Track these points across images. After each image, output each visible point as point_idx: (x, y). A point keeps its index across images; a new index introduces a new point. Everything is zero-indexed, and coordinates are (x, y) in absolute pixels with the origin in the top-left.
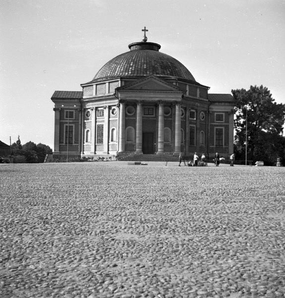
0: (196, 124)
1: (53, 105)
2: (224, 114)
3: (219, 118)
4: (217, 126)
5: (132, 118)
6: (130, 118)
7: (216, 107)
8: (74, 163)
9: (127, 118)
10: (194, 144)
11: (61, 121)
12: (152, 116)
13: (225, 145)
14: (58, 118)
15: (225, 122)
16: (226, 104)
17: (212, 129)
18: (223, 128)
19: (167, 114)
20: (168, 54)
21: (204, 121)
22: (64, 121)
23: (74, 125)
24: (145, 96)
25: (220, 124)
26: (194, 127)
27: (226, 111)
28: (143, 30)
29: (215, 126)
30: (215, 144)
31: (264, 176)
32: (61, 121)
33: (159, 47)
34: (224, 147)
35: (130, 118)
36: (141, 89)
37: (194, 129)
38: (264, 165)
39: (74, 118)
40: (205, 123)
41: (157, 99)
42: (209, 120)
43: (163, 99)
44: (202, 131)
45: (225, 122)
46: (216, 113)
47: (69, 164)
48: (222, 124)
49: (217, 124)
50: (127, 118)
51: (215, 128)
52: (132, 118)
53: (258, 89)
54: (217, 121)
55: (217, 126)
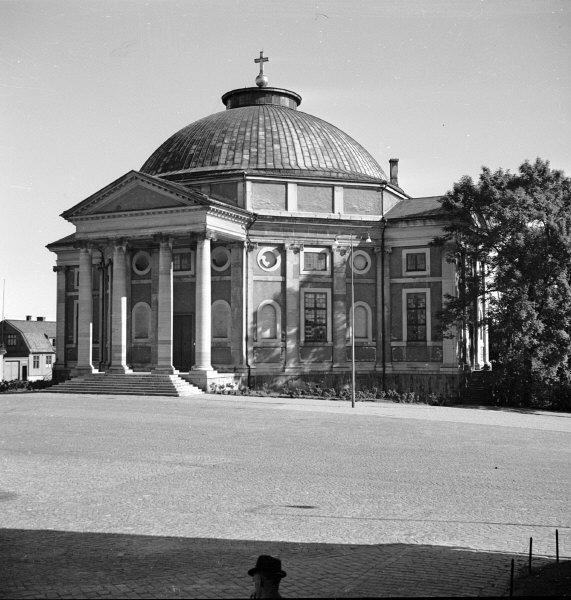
1: (52, 258)
4: (411, 286)
5: (146, 282)
6: (143, 282)
7: (404, 234)
8: (85, 395)
9: (134, 282)
11: (70, 294)
12: (187, 273)
13: (434, 338)
14: (63, 287)
15: (433, 275)
16: (428, 223)
18: (428, 291)
19: (221, 266)
21: (367, 276)
24: (127, 225)
25: (417, 280)
26: (408, 295)
28: (256, 61)
29: (405, 285)
30: (405, 338)
31: (553, 424)
32: (70, 294)
34: (429, 343)
35: (143, 282)
36: (119, 209)
38: (242, 392)
40: (370, 281)
41: (151, 232)
42: (387, 270)
43: (164, 231)
45: (433, 275)
46: (405, 253)
47: (33, 398)
48: (422, 280)
50: (134, 282)
51: (405, 292)
52: (146, 282)
53: (530, 168)
54: (410, 274)
55: (411, 286)
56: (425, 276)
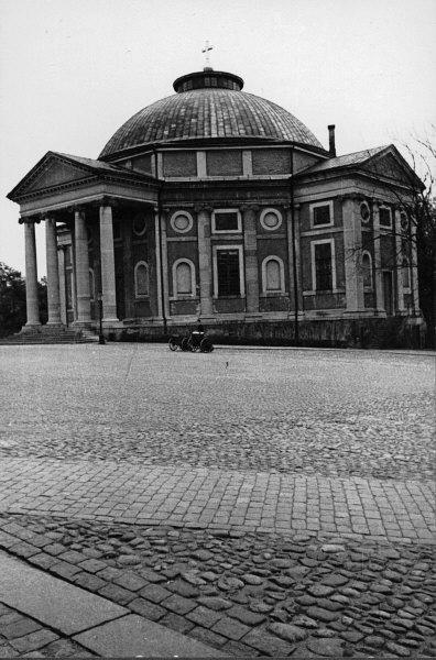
0: (242, 242)
2: (331, 203)
3: (322, 215)
9: (195, 239)
10: (332, 289)
13: (338, 287)
15: (335, 226)
17: (304, 248)
20: (24, 252)
22: (307, 234)
23: (331, 241)
25: (322, 232)
27: (334, 194)
30: (314, 287)
33: (239, 83)
34: (335, 291)
37: (237, 257)
39: (332, 223)
44: (144, 263)
45: (335, 226)
49: (318, 233)
56: (329, 228)
